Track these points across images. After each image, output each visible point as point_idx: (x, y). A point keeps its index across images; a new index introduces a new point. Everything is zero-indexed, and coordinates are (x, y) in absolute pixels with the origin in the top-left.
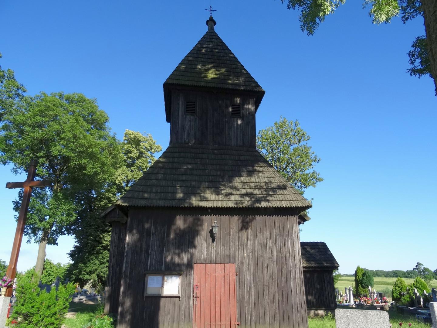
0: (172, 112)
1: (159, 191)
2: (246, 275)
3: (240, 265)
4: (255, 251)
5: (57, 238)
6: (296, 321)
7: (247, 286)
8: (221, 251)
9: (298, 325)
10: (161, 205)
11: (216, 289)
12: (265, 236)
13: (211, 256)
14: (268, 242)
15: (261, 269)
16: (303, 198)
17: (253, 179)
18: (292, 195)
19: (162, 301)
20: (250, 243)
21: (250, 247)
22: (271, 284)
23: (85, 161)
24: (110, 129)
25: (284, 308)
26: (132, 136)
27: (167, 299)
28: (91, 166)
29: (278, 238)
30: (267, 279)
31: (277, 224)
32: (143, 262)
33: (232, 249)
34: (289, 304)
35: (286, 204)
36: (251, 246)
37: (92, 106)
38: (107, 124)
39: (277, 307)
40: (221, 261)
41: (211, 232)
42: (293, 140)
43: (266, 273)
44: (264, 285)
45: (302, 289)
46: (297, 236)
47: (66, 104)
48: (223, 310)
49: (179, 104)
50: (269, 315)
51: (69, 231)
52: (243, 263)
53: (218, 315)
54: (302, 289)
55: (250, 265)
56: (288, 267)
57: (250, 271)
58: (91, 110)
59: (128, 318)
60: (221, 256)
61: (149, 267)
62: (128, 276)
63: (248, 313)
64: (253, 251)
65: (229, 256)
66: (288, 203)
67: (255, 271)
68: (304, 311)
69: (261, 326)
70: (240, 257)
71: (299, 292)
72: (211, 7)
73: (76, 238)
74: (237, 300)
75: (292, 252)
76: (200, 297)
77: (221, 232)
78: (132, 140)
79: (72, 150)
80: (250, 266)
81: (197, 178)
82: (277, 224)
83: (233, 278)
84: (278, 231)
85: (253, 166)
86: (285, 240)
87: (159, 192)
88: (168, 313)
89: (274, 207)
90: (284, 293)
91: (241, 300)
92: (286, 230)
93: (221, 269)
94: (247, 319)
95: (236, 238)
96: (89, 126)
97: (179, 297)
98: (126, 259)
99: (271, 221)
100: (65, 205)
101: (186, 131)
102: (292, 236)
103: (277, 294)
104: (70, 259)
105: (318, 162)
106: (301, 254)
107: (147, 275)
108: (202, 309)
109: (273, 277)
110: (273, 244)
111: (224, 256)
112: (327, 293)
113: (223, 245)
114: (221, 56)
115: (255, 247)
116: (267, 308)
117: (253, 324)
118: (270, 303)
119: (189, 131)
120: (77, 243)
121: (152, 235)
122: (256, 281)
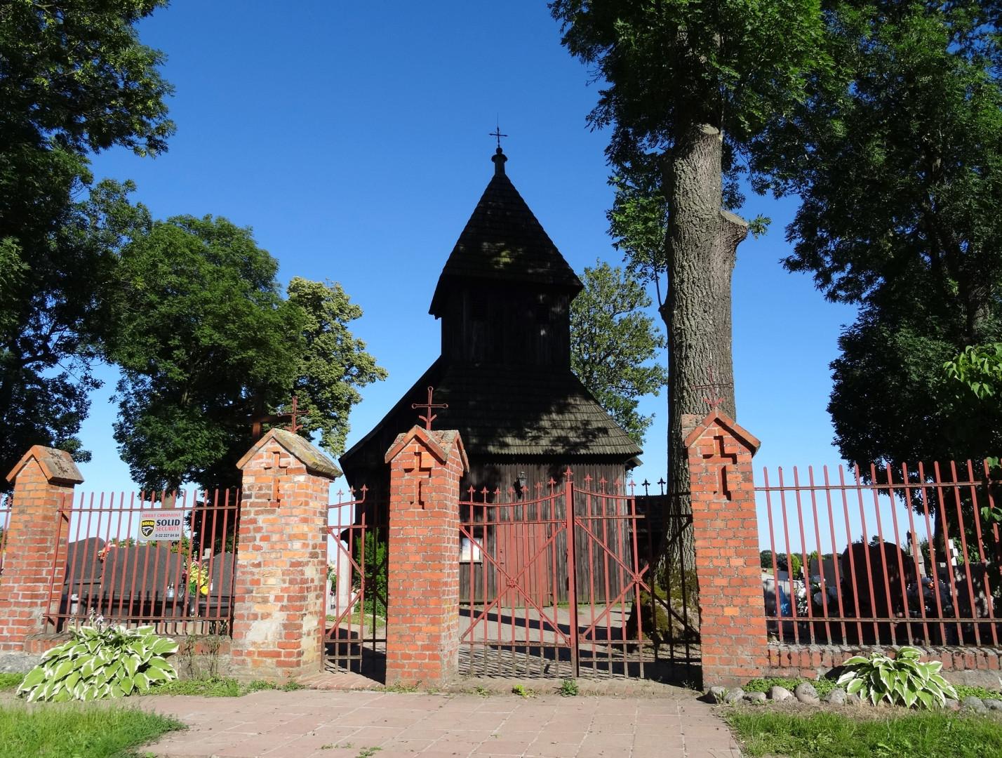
17: (567, 416)
23: (251, 353)
26: (309, 291)
41: (517, 486)
78: (307, 298)
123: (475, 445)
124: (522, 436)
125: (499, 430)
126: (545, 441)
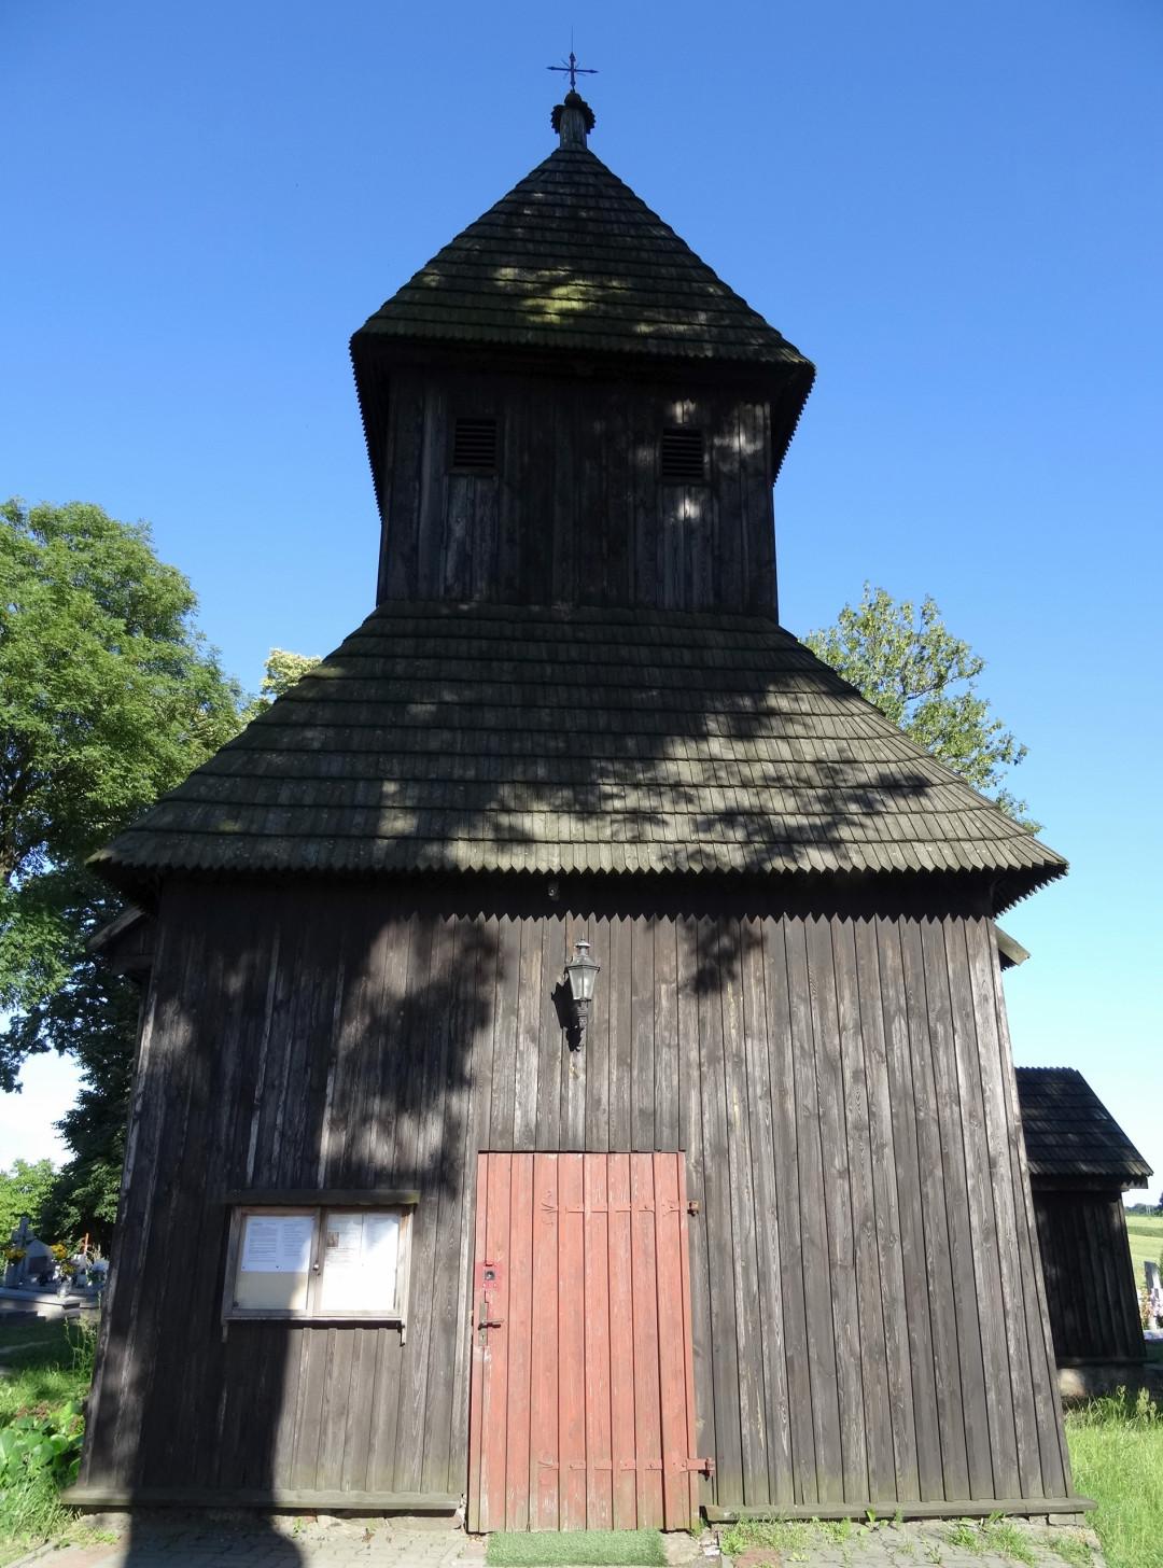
0: (390, 465)
1: (308, 800)
2: (741, 1209)
3: (707, 1159)
4: (783, 1093)
5: (20, 1064)
6: (1004, 1453)
7: (746, 1269)
8: (614, 1088)
9: (1015, 1476)
10: (313, 865)
11: (588, 1284)
12: (832, 1015)
13: (563, 1117)
14: (851, 1049)
15: (816, 1183)
16: (1022, 831)
17: (762, 748)
18: (962, 815)
19: (305, 1353)
20: (756, 1051)
21: (757, 1071)
22: (871, 1259)
23: (92, 752)
24: (201, 637)
25: (940, 1386)
27: (338, 1333)
28: (117, 772)
29: (899, 1025)
30: (850, 1235)
31: (892, 959)
32: (224, 1147)
33: (668, 1083)
34: (966, 1363)
35: (935, 857)
36: (762, 1066)
37: (129, 547)
38: (187, 619)
39: (904, 1378)
40: (612, 1142)
41: (565, 1003)
42: (915, 677)
43: (843, 1204)
44: (831, 1266)
45: (1030, 1289)
46: (994, 1017)
47: (30, 539)
48: (623, 1392)
49: (421, 429)
50: (861, 1421)
51: (65, 1039)
52: (722, 1152)
53: (597, 1417)
54: (1030, 1289)
55: (759, 1159)
56: (953, 1171)
57: (757, 1193)
58: (123, 563)
59: (125, 1445)
60: (614, 1117)
61: (250, 1169)
62: (146, 1217)
63: (752, 1413)
64: (776, 1092)
65: (651, 1116)
66: (947, 851)
67: (788, 1194)
68: (1046, 1404)
69: (825, 1481)
70: (709, 1121)
71: (1018, 1301)
72: (572, 58)
73: (87, 1060)
74: (695, 1342)
75: (973, 1097)
76: (504, 1325)
77: (614, 996)
79: (40, 709)
80: (761, 1169)
81: (494, 742)
82: (892, 959)
83: (672, 1227)
84: (897, 992)
85: (761, 693)
86: (932, 1036)
87: (309, 806)
88: (344, 1411)
89: (877, 868)
90: (937, 1306)
91: (719, 1341)
92: (938, 986)
93: (611, 1180)
94: (747, 1441)
95: (686, 1027)
96: (116, 625)
97: (396, 1326)
98: (140, 1129)
99: (858, 940)
100: (22, 932)
101: (454, 546)
102: (967, 1015)
103: (901, 1313)
104: (64, 1143)
105: (1016, 762)
106: (1016, 1108)
107: (238, 1213)
108: (518, 1392)
109: (881, 1224)
110: (875, 1057)
111: (627, 1117)
112: (1099, 1292)
113: (621, 1061)
114: (615, 235)
115: (781, 1072)
116: (854, 1387)
117: (783, 1473)
118: (865, 1359)
119: (468, 548)
120: (87, 1081)
121: (269, 1010)
122: (791, 1243)
123: (402, 839)
124: (587, 811)
125: (505, 791)
126: (677, 828)
